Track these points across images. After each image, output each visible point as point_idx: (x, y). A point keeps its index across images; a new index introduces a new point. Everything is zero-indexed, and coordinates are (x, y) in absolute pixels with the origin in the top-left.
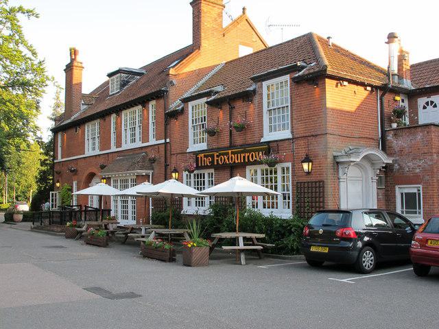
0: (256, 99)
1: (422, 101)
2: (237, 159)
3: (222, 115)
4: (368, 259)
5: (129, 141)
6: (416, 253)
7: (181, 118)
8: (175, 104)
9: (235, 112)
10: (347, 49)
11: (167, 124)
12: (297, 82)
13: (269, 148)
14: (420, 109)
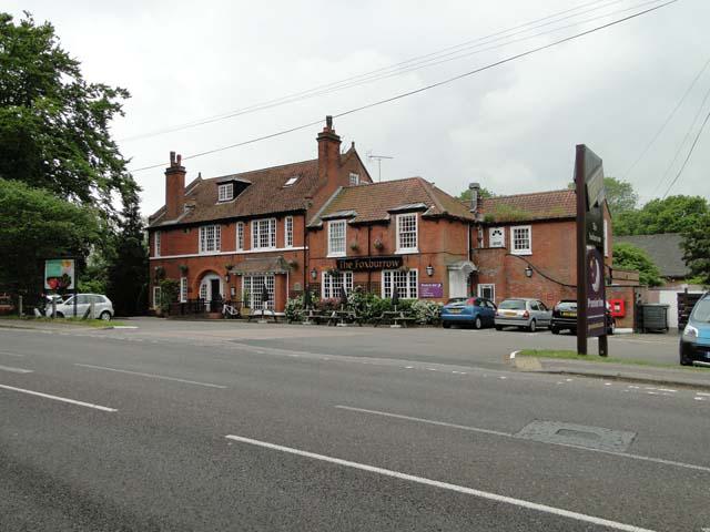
0: (390, 227)
1: (492, 230)
2: (373, 264)
3: (363, 234)
4: (478, 323)
5: (206, 247)
6: (92, 268)
7: (319, 234)
8: (313, 221)
9: (373, 234)
10: (531, 192)
11: (305, 236)
12: (352, 225)
13: (400, 259)
14: (491, 235)
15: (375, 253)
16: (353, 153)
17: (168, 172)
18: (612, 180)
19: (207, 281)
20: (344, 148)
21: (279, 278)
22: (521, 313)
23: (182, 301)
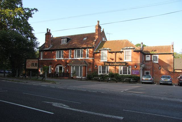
1: (147, 56)
2: (117, 64)
14: (146, 57)
15: (118, 60)
16: (103, 32)
17: (46, 34)
18: (31, 29)
19: (58, 67)
20: (102, 30)
21: (84, 67)
22: (150, 79)
23: (50, 73)
